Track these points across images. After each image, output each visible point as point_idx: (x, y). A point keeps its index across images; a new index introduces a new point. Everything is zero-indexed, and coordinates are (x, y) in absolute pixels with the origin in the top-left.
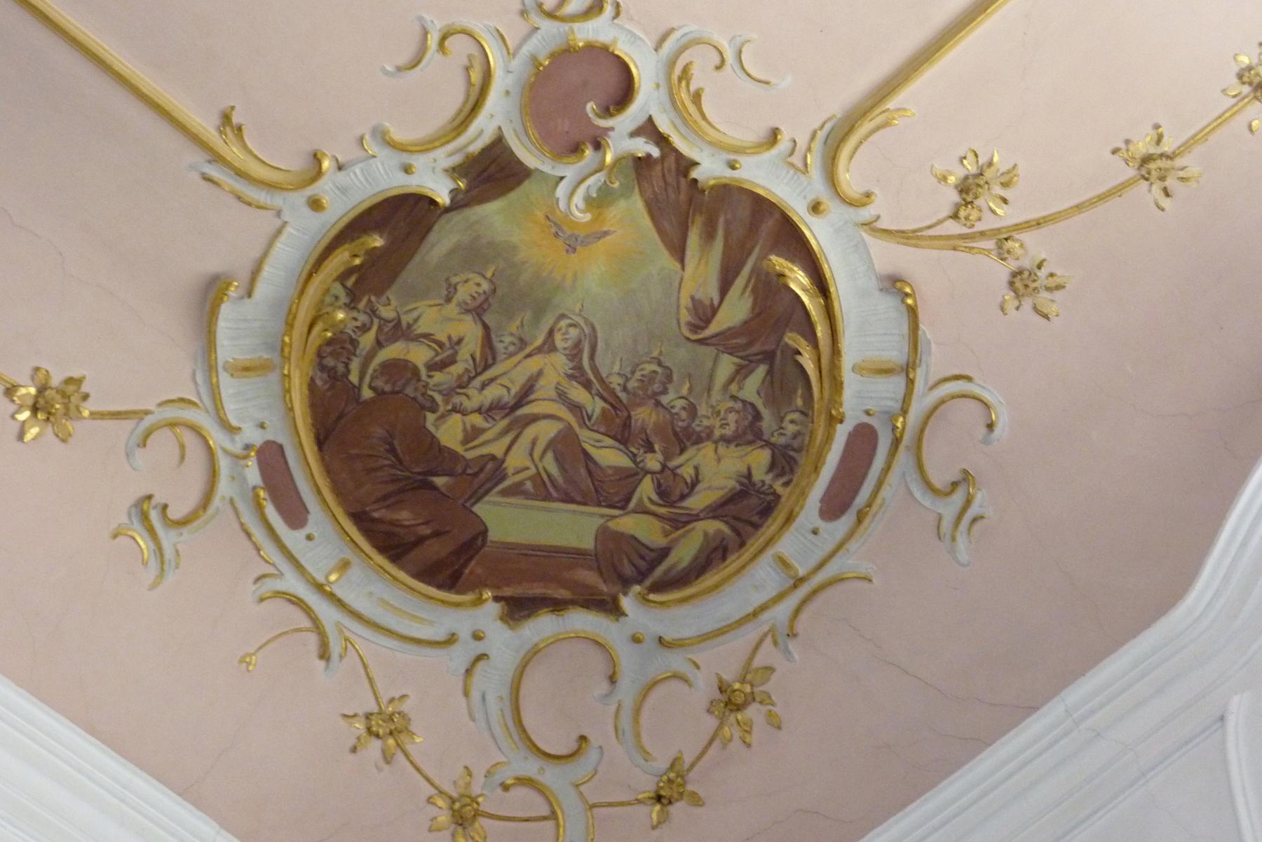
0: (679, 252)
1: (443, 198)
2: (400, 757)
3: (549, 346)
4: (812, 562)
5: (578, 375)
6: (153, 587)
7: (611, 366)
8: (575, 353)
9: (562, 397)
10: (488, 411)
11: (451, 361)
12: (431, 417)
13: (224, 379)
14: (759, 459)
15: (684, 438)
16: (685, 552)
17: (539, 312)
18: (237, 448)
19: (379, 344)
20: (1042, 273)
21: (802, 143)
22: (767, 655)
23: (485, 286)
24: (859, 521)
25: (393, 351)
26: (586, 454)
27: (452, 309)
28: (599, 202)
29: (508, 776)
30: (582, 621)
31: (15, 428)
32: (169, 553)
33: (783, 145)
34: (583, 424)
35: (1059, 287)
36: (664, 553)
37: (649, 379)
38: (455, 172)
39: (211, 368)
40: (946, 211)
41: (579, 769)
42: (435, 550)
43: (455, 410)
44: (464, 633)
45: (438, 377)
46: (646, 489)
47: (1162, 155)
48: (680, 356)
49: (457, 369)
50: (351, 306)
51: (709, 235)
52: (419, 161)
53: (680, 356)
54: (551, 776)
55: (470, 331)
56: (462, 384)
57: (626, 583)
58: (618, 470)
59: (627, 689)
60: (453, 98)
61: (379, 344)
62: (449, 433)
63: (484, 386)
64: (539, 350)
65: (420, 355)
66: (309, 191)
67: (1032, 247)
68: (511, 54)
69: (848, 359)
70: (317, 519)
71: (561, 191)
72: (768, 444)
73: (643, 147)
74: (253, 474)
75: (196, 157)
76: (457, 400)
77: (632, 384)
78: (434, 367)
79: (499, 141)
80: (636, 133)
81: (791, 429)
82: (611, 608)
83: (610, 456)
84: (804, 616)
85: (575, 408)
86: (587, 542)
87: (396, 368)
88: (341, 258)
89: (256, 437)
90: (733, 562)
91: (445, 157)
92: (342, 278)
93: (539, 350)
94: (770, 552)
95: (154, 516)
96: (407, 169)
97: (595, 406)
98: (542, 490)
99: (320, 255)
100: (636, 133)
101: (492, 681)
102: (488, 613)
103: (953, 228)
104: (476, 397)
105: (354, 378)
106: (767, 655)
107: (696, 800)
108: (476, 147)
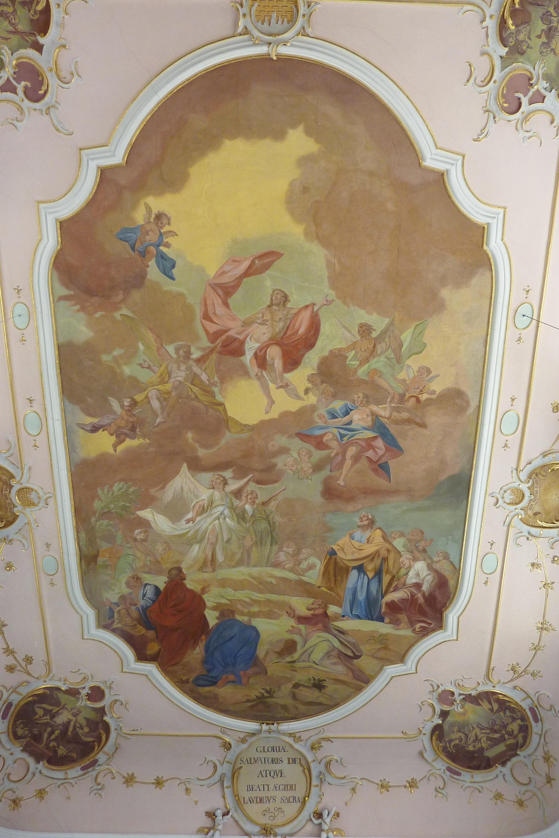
0: (480, 705)
1: (441, 722)
2: (504, 800)
3: (473, 728)
4: (540, 730)
5: (481, 729)
6: (447, 801)
7: (485, 725)
8: (478, 727)
9: (482, 733)
10: (474, 742)
11: (462, 740)
12: (466, 748)
13: (433, 763)
14: (519, 721)
15: (505, 726)
16: (520, 740)
17: (468, 726)
18: (443, 771)
19: (450, 744)
20: (535, 671)
21: (483, 681)
22: (546, 749)
23: (457, 728)
24: (542, 721)
25: (453, 744)
26: (494, 738)
27: (456, 733)
28: (463, 707)
29: (523, 792)
30: (514, 760)
31: (410, 791)
32: (445, 794)
33: (481, 683)
34: (489, 734)
35: (540, 672)
36: (517, 742)
37: (492, 723)
38: (439, 718)
39: (430, 764)
40: (513, 674)
41: (533, 783)
42: (483, 764)
43: (469, 745)
44: (499, 773)
45: (462, 742)
46: (506, 736)
47: (537, 646)
48: (494, 717)
49: (464, 740)
50: (441, 742)
51: (482, 700)
52: (433, 720)
53: (494, 717)
54: (529, 787)
55: (460, 734)
56: (466, 741)
57: (516, 750)
58: (500, 737)
59: (530, 766)
60: (430, 710)
61: (450, 744)
62: (471, 748)
63: (470, 739)
64: (473, 730)
65: (457, 742)
66: (422, 733)
67: (531, 669)
68: (432, 699)
69: (519, 702)
70: (463, 773)
71: (456, 709)
72: (518, 719)
73: (462, 697)
74: (448, 773)
75: (403, 740)
76: (468, 744)
77: (490, 725)
78: (460, 742)
79: (441, 710)
80: (459, 696)
81: (519, 715)
82: (516, 755)
83: (496, 736)
84: (546, 738)
85: (485, 733)
86: (505, 748)
87: (455, 746)
88: (434, 738)
89: (444, 768)
90: (529, 737)
91: (436, 717)
92: (437, 740)
93: (473, 730)
94: (533, 733)
95: (439, 790)
96: (433, 722)
97: (488, 731)
98: (491, 746)
99: (556, 179)
100: (459, 696)
101: (509, 778)
102: (500, 768)
103: (516, 676)
104: (470, 742)
105: (451, 751)
106: (546, 749)
107: (554, 780)
108: (439, 713)
